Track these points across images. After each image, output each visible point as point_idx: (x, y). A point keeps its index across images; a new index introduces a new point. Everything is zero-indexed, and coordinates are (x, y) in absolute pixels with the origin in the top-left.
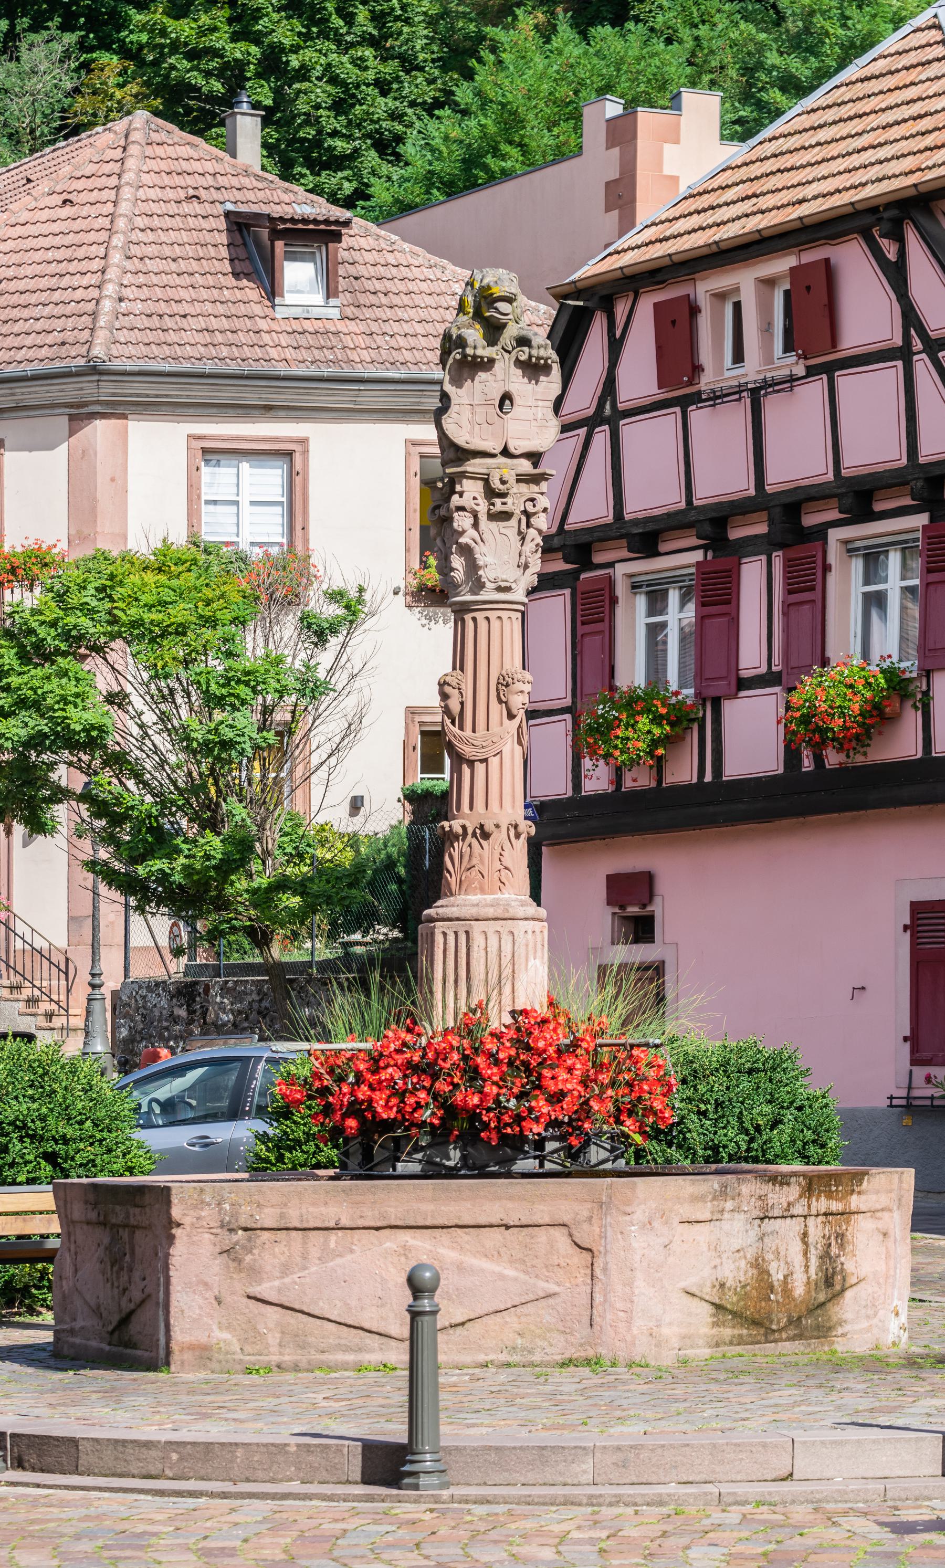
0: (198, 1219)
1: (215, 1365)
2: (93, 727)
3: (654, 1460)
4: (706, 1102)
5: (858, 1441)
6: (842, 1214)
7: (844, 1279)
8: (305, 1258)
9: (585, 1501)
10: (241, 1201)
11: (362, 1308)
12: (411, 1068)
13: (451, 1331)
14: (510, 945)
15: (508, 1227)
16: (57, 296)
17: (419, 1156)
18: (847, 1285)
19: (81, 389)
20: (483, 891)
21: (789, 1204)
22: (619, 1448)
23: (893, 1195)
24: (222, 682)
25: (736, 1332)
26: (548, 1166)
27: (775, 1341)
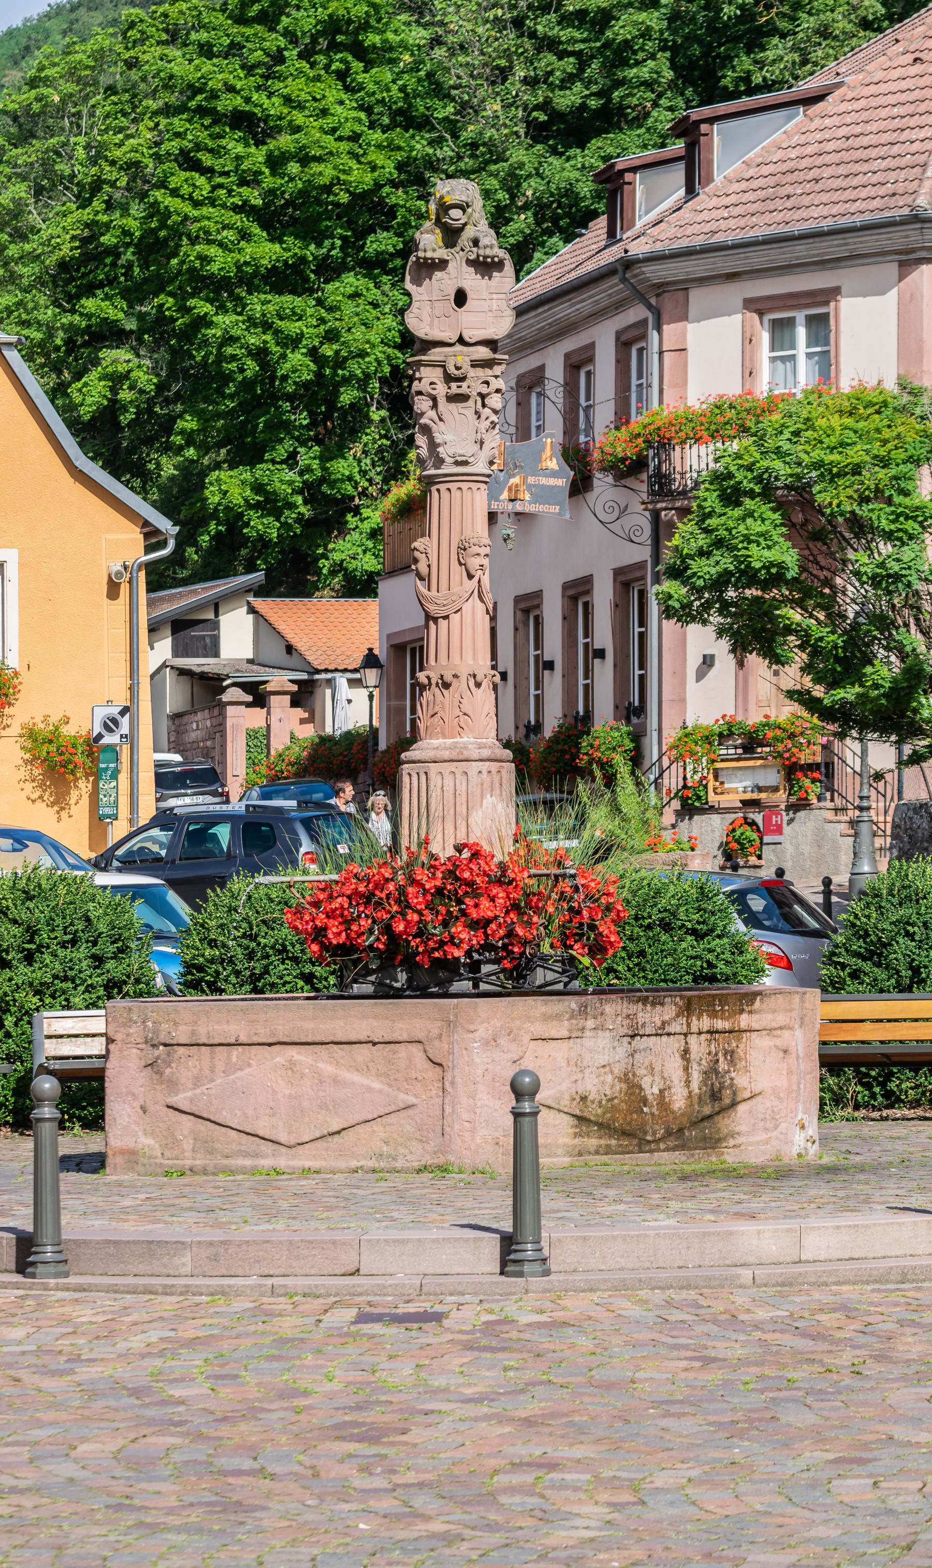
0: (128, 1035)
1: (140, 1169)
2: (772, 564)
3: (240, 1255)
4: (913, 925)
5: (419, 1240)
6: (730, 1032)
7: (734, 1094)
8: (212, 1072)
9: (160, 1291)
10: (161, 1019)
11: (257, 1118)
12: (354, 896)
13: (330, 1139)
14: (464, 784)
15: (374, 1044)
16: (895, 150)
17: (372, 978)
18: (739, 1099)
19: (907, 237)
20: (444, 737)
21: (664, 1023)
22: (211, 1244)
23: (793, 1014)
24: (891, 517)
25: (603, 1142)
26: (483, 987)
27: (651, 1151)
